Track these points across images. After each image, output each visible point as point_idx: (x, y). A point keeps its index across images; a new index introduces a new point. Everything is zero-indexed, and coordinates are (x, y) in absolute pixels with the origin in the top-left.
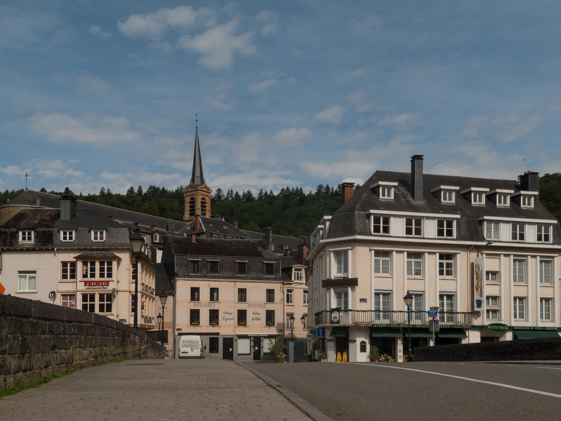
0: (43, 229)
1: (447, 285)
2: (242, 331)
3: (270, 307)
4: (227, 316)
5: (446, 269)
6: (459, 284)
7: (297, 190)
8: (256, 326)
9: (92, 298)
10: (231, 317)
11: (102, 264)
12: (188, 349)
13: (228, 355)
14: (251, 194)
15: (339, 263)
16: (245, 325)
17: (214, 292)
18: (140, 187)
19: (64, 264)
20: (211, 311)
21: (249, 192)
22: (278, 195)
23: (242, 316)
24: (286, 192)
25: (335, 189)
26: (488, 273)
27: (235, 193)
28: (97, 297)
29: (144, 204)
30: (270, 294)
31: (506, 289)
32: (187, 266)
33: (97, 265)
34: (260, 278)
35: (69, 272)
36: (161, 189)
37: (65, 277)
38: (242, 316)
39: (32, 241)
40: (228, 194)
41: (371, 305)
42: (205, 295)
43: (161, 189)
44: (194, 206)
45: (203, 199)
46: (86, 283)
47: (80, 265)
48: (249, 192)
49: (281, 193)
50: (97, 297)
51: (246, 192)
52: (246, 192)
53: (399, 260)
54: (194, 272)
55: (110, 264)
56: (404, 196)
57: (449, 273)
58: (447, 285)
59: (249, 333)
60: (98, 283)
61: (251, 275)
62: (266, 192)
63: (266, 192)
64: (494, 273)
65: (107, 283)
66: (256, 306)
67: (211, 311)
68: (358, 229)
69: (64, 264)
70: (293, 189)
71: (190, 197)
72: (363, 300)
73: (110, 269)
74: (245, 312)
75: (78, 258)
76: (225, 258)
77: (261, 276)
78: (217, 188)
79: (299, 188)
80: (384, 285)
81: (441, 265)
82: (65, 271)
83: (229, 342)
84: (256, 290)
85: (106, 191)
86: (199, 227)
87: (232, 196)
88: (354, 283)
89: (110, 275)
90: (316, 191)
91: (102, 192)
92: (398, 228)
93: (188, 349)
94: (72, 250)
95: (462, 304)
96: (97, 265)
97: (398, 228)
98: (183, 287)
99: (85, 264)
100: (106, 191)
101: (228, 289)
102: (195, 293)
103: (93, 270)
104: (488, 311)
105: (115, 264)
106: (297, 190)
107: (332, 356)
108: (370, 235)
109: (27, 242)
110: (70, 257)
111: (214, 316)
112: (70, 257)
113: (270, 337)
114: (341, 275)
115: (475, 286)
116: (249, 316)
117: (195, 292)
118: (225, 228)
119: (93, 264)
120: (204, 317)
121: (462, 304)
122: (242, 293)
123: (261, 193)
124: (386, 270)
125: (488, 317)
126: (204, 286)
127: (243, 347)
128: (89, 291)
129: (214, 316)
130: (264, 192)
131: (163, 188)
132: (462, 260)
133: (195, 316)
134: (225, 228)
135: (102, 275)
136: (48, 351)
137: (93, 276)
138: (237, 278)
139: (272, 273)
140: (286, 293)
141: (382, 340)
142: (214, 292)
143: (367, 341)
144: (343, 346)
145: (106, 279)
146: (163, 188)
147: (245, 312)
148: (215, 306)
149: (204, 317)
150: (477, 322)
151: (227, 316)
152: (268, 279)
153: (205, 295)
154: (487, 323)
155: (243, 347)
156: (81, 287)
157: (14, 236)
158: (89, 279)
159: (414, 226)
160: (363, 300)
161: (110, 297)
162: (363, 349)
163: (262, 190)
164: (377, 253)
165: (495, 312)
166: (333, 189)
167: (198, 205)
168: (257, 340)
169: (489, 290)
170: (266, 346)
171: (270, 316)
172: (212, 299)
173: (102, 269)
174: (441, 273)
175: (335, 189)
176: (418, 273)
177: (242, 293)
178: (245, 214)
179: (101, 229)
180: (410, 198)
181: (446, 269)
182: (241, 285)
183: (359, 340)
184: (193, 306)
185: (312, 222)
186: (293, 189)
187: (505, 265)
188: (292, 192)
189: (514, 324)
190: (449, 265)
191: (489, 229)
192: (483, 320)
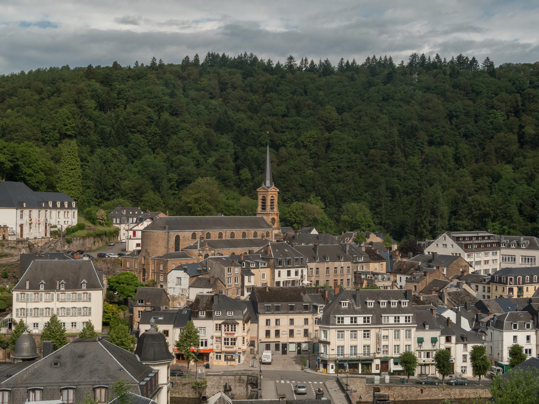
0: (208, 311)
1: (367, 342)
2: (291, 340)
3: (306, 327)
4: (284, 333)
5: (367, 335)
6: (372, 341)
7: (386, 59)
8: (299, 338)
9: (228, 339)
10: (286, 333)
11: (232, 326)
12: (266, 359)
13: (284, 352)
14: (330, 64)
15: (325, 334)
16: (293, 337)
17: (277, 322)
18: (197, 55)
19: (217, 325)
20: (276, 331)
21: (327, 61)
22: (363, 65)
23: (291, 332)
24: (372, 62)
25: (432, 60)
26: (384, 336)
27: (309, 62)
28: (230, 339)
29: (202, 79)
30: (306, 321)
31: (391, 342)
32: (264, 309)
33: (230, 326)
34: (301, 313)
35: (218, 327)
36: (221, 55)
37: (216, 330)
38: (291, 332)
39: (204, 316)
40: (302, 63)
41: (335, 352)
42: (273, 323)
43: (221, 55)
44: (265, 203)
45: (272, 197)
46: (226, 334)
47: (223, 326)
48: (327, 61)
49: (366, 64)
50: (230, 339)
51: (323, 61)
52: (323, 61)
53: (347, 334)
54: (267, 311)
55: (235, 326)
56: (353, 305)
57: (368, 337)
58: (367, 342)
59: (295, 341)
60: (230, 334)
61: (296, 311)
62: (348, 62)
63: (348, 62)
64: (387, 337)
65: (234, 334)
66: (298, 327)
67: (276, 331)
68: (331, 323)
69: (217, 325)
70: (381, 58)
71: (262, 196)
72: (333, 350)
73: (235, 328)
74: (293, 330)
75: (223, 323)
76: (283, 303)
77: (302, 311)
78: (289, 56)
79: (388, 58)
80: (341, 343)
81: (364, 334)
82: (217, 327)
83: (285, 346)
84: (299, 319)
85: (158, 62)
86: (269, 253)
87: (305, 66)
88: (329, 343)
89: (235, 331)
90: (409, 61)
91: (153, 64)
92: (347, 321)
93: (266, 359)
94: (220, 319)
95: (373, 350)
96: (230, 326)
97: (347, 321)
98: (262, 319)
99: (225, 326)
100: (158, 62)
101: (285, 319)
102: (268, 322)
103: (228, 328)
104: (384, 351)
105: (237, 326)
106: (386, 59)
107: (322, 369)
108: (336, 325)
109: (202, 316)
110: (220, 322)
111: (277, 333)
112: (220, 322)
113: (305, 342)
114: (325, 339)
115: (378, 342)
116: (295, 332)
117: (268, 322)
118: (286, 250)
119: (228, 326)
120: (273, 334)
121: (373, 350)
122: (292, 321)
123: (342, 62)
124: (342, 337)
125: (383, 353)
126: (273, 318)
127: (292, 348)
128: (227, 337)
129: (277, 333)
130: (345, 61)
131: (224, 55)
132: (373, 333)
133: (268, 333)
134: (286, 250)
135: (232, 331)
136: (148, 303)
137: (228, 330)
138: (289, 313)
139: (307, 310)
140: (314, 320)
141: (340, 365)
142: (277, 322)
143: (334, 365)
144: (325, 366)
145: (233, 332)
146: (224, 55)
147: (293, 330)
148: (278, 328)
149: (273, 334)
150: (377, 356)
151: (284, 333)
152: (305, 313)
153: (273, 323)
154: (383, 356)
155: (292, 348)
156: (224, 335)
157: (197, 313)
158: (227, 332)
159: (354, 320)
160: (333, 350)
161: (235, 339)
162: (332, 368)
163: (342, 59)
164: (338, 331)
165: (387, 351)
166: (429, 59)
167: (268, 203)
168: (299, 345)
169: (384, 343)
170: (304, 346)
171: (306, 332)
172: (276, 324)
173: (232, 328)
174: (364, 337)
175: (432, 60)
176: (355, 338)
177: (292, 321)
178: (321, 93)
179: (231, 311)
180: (355, 306)
181: (367, 335)
182: (291, 317)
183: (331, 364)
184: (267, 328)
185: (401, 107)
186: (381, 58)
187: (391, 333)
188: (377, 63)
189: (394, 356)
190: (368, 334)
191: (385, 319)
192: (381, 355)
